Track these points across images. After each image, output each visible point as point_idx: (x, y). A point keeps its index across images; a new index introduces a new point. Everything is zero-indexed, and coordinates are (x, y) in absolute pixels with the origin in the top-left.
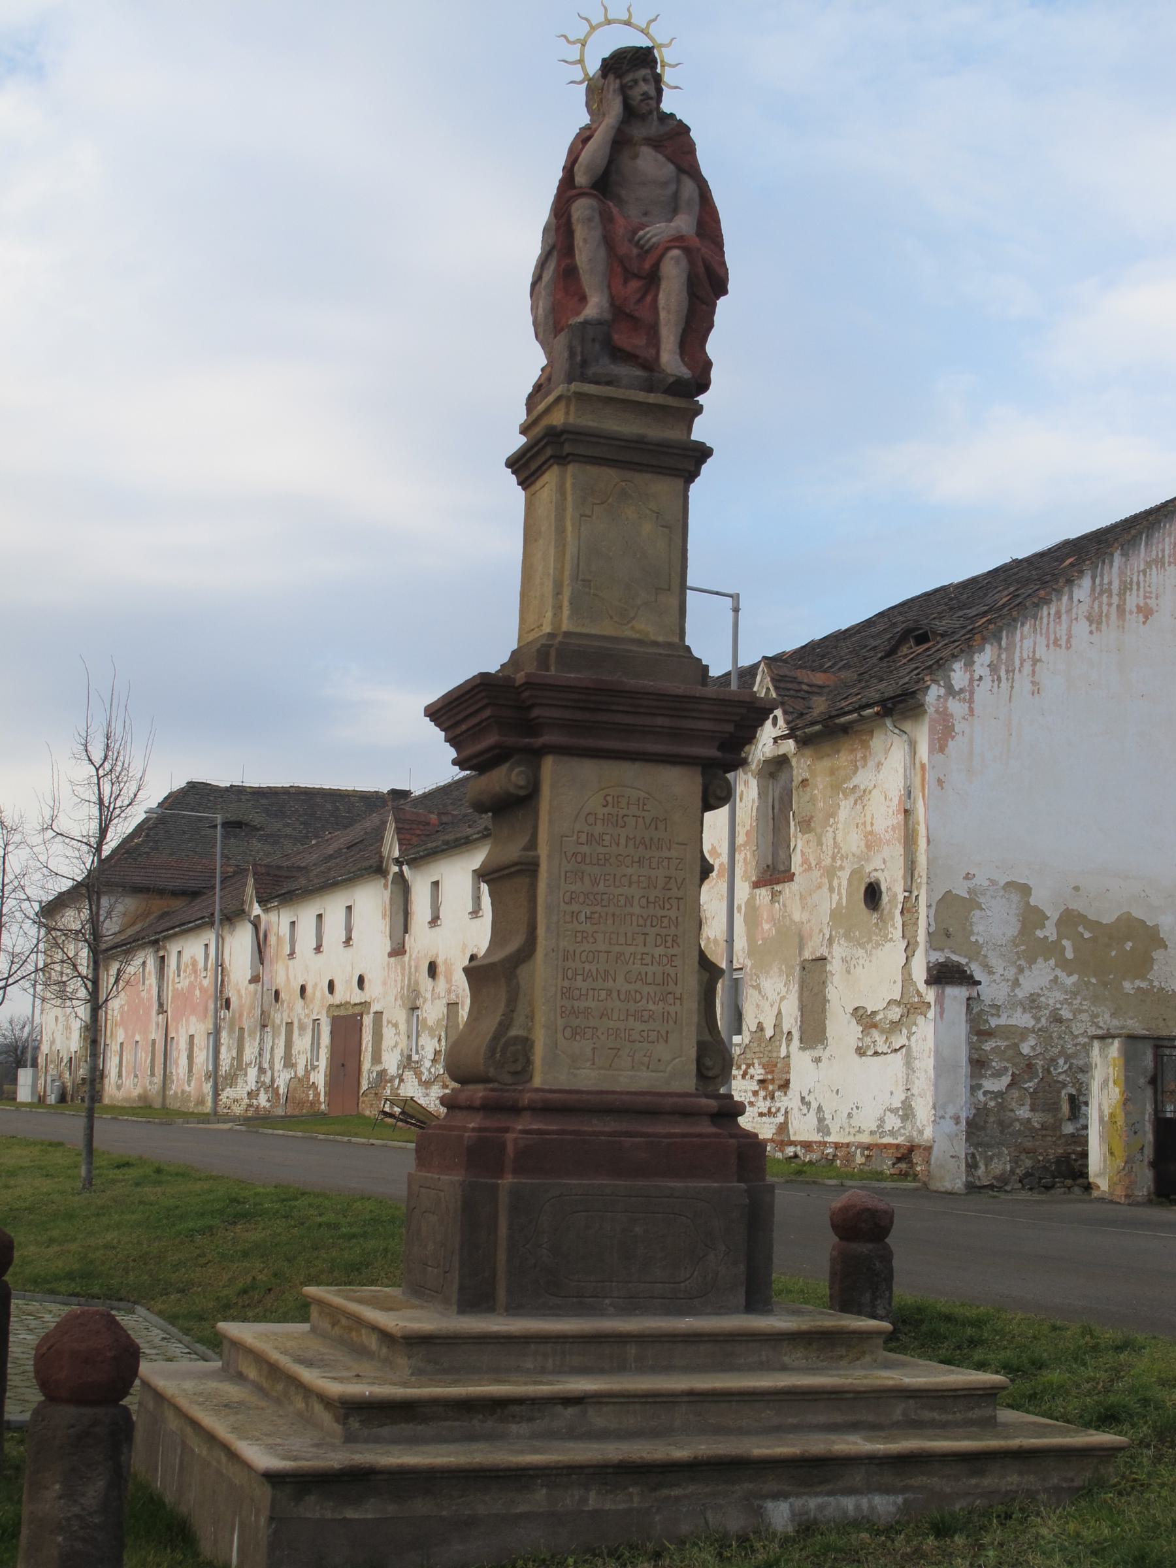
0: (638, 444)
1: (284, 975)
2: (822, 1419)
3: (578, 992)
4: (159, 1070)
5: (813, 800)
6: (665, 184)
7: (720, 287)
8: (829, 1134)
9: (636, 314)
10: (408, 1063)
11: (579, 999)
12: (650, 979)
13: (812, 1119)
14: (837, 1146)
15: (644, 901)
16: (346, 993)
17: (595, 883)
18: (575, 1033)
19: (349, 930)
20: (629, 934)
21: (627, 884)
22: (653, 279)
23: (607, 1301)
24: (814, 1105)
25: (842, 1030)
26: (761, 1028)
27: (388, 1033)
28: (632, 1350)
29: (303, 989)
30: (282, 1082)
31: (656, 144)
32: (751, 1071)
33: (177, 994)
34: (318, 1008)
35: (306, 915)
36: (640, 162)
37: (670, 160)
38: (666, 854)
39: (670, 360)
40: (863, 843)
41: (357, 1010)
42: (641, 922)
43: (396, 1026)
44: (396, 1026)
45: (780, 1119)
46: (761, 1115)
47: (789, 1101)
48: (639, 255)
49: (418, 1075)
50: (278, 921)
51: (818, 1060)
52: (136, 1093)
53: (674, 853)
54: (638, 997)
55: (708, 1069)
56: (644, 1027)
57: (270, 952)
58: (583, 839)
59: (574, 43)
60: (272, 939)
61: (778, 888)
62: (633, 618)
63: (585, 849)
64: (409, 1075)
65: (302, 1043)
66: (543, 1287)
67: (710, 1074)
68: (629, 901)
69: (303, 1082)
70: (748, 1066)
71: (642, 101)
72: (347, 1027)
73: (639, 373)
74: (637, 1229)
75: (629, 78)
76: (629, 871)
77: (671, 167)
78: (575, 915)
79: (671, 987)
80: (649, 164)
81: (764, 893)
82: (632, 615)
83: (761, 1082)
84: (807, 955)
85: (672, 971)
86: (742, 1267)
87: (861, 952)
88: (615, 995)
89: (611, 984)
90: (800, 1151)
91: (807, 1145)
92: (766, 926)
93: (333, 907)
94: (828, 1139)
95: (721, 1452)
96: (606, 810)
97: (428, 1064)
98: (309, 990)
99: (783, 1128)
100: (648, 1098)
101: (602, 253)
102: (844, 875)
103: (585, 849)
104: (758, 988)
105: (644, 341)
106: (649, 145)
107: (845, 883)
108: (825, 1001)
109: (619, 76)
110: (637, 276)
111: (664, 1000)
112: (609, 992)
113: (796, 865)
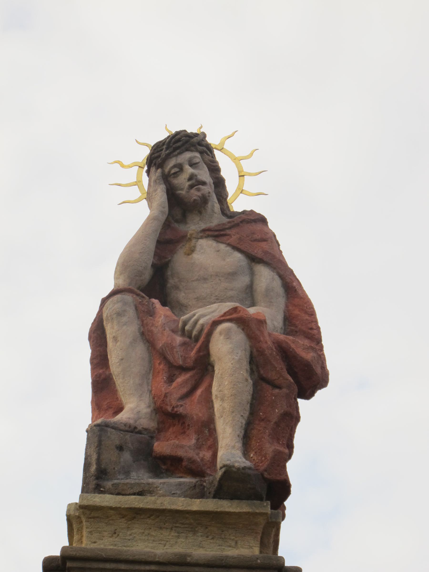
6: (232, 275)
7: (310, 378)
9: (181, 410)
22: (203, 367)
31: (217, 234)
36: (197, 256)
37: (235, 248)
48: (184, 344)
59: (130, 167)
71: (191, 187)
73: (188, 480)
75: (172, 162)
77: (238, 255)
101: (140, 350)
105: (194, 441)
106: (207, 237)
109: (161, 166)
110: (183, 369)
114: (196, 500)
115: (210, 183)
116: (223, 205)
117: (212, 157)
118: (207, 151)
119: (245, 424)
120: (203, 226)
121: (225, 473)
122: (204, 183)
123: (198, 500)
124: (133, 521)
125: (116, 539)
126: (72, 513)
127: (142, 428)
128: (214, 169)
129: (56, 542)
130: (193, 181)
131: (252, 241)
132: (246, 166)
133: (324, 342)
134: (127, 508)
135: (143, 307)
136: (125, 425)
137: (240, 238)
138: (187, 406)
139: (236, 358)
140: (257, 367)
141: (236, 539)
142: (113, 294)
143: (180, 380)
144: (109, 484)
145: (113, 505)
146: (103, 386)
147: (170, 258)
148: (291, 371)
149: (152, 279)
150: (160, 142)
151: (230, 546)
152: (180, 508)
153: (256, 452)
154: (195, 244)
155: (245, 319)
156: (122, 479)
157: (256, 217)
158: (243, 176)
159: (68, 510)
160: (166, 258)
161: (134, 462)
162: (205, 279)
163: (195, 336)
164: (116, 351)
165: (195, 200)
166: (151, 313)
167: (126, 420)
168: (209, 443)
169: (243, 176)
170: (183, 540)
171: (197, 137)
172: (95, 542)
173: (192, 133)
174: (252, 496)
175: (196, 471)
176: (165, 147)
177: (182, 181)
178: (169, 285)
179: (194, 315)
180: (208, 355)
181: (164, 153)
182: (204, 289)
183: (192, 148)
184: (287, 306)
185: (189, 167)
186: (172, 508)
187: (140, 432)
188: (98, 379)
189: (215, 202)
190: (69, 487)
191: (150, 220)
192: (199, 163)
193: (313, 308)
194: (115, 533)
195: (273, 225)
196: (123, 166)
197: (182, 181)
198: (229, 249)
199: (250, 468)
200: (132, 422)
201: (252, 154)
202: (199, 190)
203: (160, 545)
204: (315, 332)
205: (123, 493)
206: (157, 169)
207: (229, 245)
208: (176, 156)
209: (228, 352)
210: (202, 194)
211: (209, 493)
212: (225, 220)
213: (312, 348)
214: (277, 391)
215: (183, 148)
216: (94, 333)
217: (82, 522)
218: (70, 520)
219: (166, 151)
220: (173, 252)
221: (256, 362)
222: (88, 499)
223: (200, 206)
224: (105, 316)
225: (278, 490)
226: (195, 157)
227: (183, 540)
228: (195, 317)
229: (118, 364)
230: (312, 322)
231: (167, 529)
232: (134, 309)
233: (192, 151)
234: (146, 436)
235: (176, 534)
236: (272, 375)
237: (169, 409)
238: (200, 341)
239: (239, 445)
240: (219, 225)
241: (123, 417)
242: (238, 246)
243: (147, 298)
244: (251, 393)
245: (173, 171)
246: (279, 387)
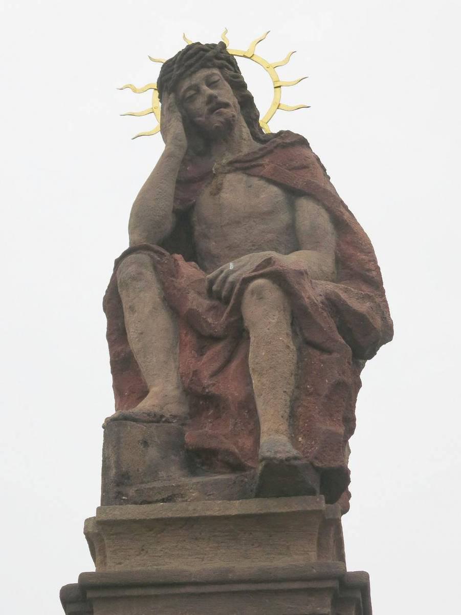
22: (238, 334)
31: (246, 166)
37: (270, 181)
71: (212, 111)
75: (186, 84)
77: (274, 189)
109: (174, 89)
110: (215, 339)
114: (235, 502)
115: (234, 103)
116: (253, 127)
117: (236, 72)
118: (227, 64)
119: (290, 401)
120: (229, 157)
121: (266, 466)
122: (226, 105)
123: (238, 502)
124: (163, 534)
125: (145, 557)
126: (90, 530)
127: (171, 415)
128: (239, 86)
129: (80, 562)
130: (213, 104)
131: (290, 170)
132: (284, 75)
133: (386, 286)
134: (154, 519)
135: (162, 267)
136: (149, 415)
137: (275, 167)
138: (220, 385)
139: (273, 321)
140: (301, 329)
141: (287, 544)
142: (126, 254)
143: (209, 354)
144: (131, 491)
145: (138, 517)
146: (125, 367)
147: (194, 201)
148: (344, 329)
149: (172, 228)
150: (171, 60)
151: (280, 554)
152: (217, 514)
153: (304, 435)
154: (222, 180)
155: (281, 272)
156: (148, 482)
157: (294, 140)
158: (280, 87)
159: (86, 528)
160: (190, 201)
161: (163, 458)
163: (224, 297)
164: (133, 325)
165: (217, 127)
166: (174, 272)
167: (148, 408)
168: (250, 427)
169: (280, 87)
170: (224, 551)
171: (213, 49)
172: (120, 563)
173: (207, 45)
176: (175, 66)
177: (200, 104)
178: (196, 233)
179: (222, 272)
180: (241, 319)
181: (176, 73)
183: (209, 64)
184: (338, 245)
185: (207, 88)
186: (207, 515)
187: (167, 421)
188: (117, 359)
189: (243, 126)
190: (86, 497)
191: (167, 156)
192: (218, 80)
193: (370, 244)
194: (143, 550)
195: (317, 147)
196: (135, 90)
198: (262, 183)
199: (295, 458)
200: (157, 410)
201: (287, 60)
202: (220, 114)
203: (197, 559)
204: (374, 273)
205: (150, 500)
206: (169, 94)
207: (262, 177)
208: (191, 75)
210: (225, 119)
211: (251, 491)
212: (259, 145)
213: (369, 297)
214: (325, 357)
215: (197, 65)
216: (108, 303)
217: (103, 540)
219: (177, 70)
222: (107, 513)
225: (335, 484)
226: (214, 74)
227: (224, 551)
228: (223, 275)
229: (137, 339)
230: (370, 261)
231: (204, 539)
232: (152, 270)
233: (209, 67)
235: (216, 545)
236: (318, 338)
237: (199, 389)
238: (229, 298)
239: (284, 427)
240: (249, 154)
241: (146, 405)
242: (273, 178)
243: (167, 253)
244: (295, 361)
245: (188, 95)
246: (330, 352)
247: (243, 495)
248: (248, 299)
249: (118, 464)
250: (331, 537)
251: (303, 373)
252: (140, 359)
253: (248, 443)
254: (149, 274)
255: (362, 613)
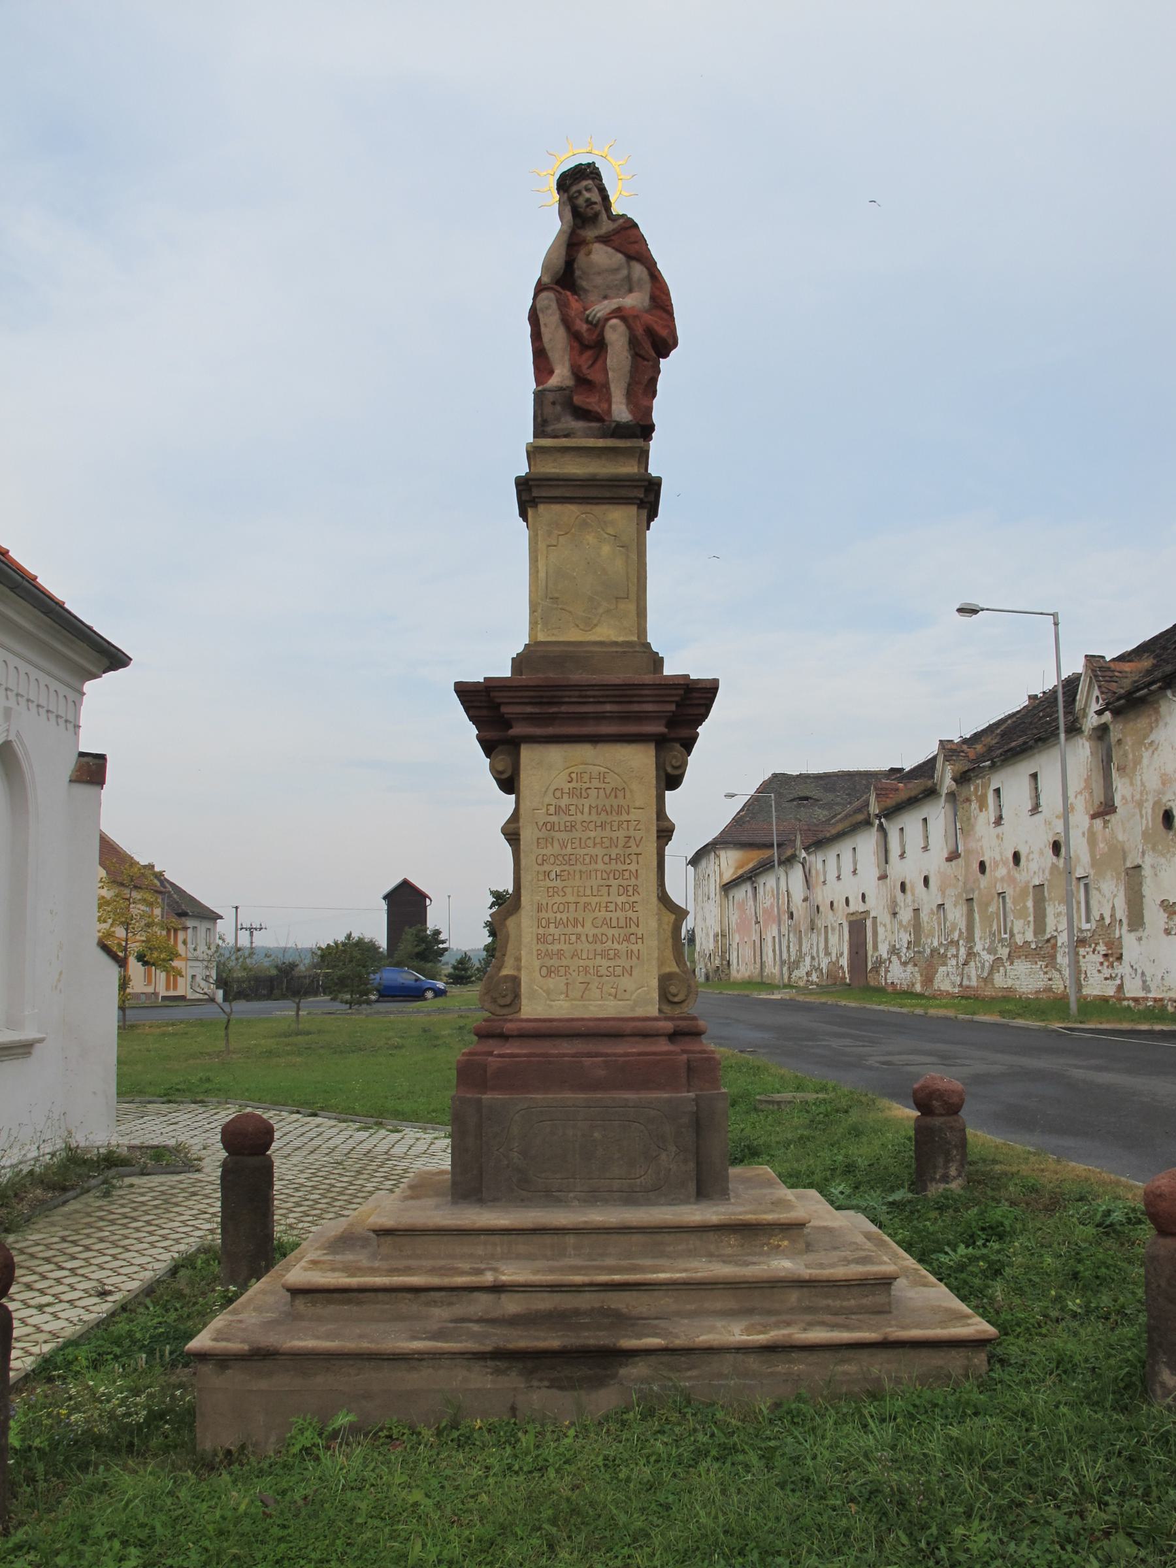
0: (591, 482)
1: (822, 896)
2: (719, 1305)
3: (550, 938)
4: (758, 960)
5: (1125, 755)
6: (617, 270)
8: (1149, 991)
10: (894, 951)
11: (552, 943)
12: (614, 924)
13: (1138, 982)
14: (1155, 1000)
15: (606, 859)
16: (856, 906)
17: (563, 846)
18: (549, 972)
19: (855, 863)
20: (595, 888)
21: (591, 845)
22: (599, 346)
23: (571, 1195)
24: (1139, 971)
25: (1154, 917)
26: (1102, 918)
27: (881, 930)
28: (571, 1240)
29: (832, 903)
30: (824, 965)
31: (605, 240)
32: (1098, 948)
33: (765, 911)
34: (839, 918)
35: (830, 855)
38: (625, 817)
39: (621, 412)
40: (1159, 782)
41: (863, 916)
42: (605, 876)
43: (885, 926)
44: (885, 926)
45: (1118, 982)
46: (1106, 979)
47: (1123, 969)
48: (588, 330)
49: (900, 958)
50: (816, 860)
51: (1140, 939)
52: (747, 974)
53: (632, 817)
54: (604, 939)
55: (675, 996)
56: (610, 963)
57: (813, 880)
58: (552, 810)
60: (813, 872)
61: (1107, 818)
62: (596, 625)
63: (554, 819)
64: (894, 958)
65: (833, 939)
66: (523, 1186)
67: (676, 999)
68: (594, 859)
69: (835, 964)
70: (1097, 944)
72: (858, 927)
74: (596, 1134)
75: (574, 189)
76: (592, 834)
77: (620, 256)
78: (547, 874)
79: (633, 929)
80: (601, 256)
81: (1099, 823)
82: (595, 622)
83: (1105, 956)
84: (1129, 865)
85: (634, 916)
86: (692, 1165)
87: (1163, 860)
88: (583, 938)
89: (580, 929)
90: (1132, 1004)
91: (1136, 1000)
92: (1101, 845)
93: (844, 848)
94: (1150, 995)
95: (592, 1342)
96: (571, 785)
97: (904, 950)
98: (835, 904)
99: (1120, 988)
100: (611, 1023)
102: (1148, 806)
103: (554, 819)
104: (1098, 889)
106: (600, 242)
107: (1150, 811)
108: (1142, 897)
111: (628, 940)
112: (579, 937)
113: (1118, 801)
149: (563, 278)
162: (599, 273)
174: (632, 436)
175: (598, 418)
180: (603, 338)
182: (599, 280)
190: (526, 434)
197: (581, 201)
209: (616, 337)
218: (528, 452)
220: (578, 251)
221: (633, 343)
223: (594, 219)
224: (538, 307)
225: (646, 430)
234: (567, 392)
236: (642, 352)
238: (597, 326)
247: (604, 436)
248: (607, 328)
249: (542, 414)
250: (643, 456)
251: (635, 370)
252: (550, 354)
253: (605, 406)
254: (554, 305)
255: (640, 443)
